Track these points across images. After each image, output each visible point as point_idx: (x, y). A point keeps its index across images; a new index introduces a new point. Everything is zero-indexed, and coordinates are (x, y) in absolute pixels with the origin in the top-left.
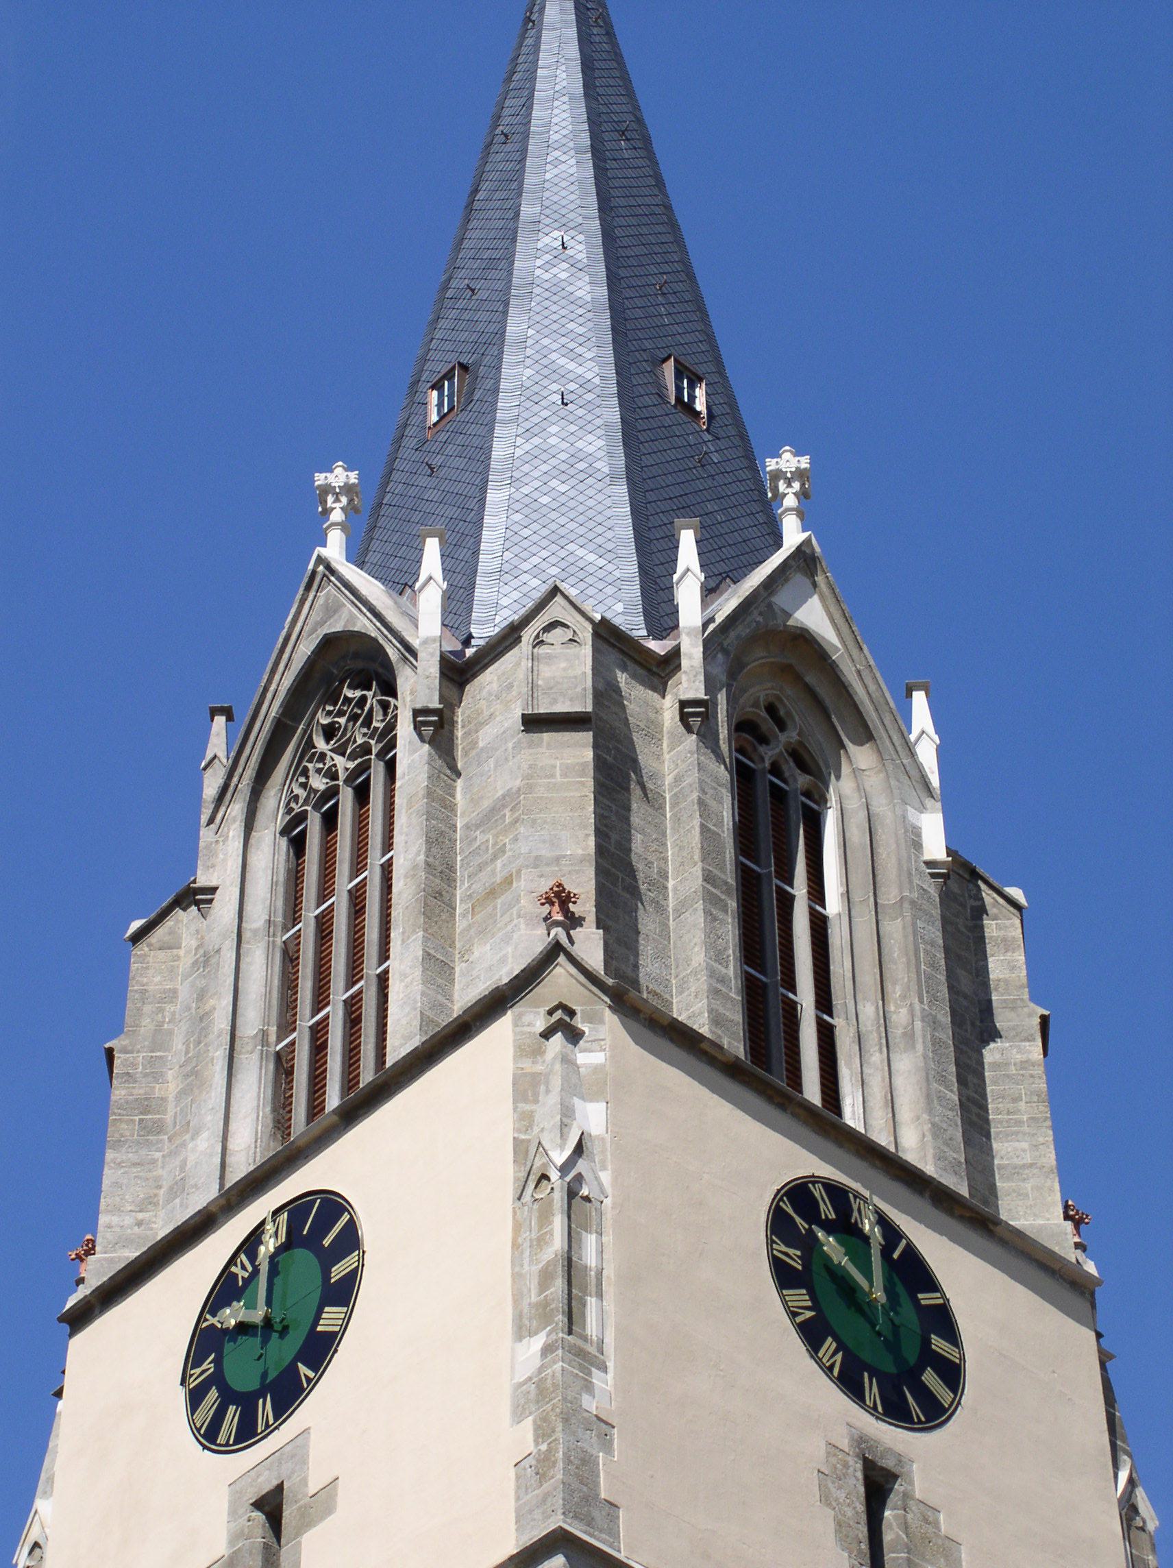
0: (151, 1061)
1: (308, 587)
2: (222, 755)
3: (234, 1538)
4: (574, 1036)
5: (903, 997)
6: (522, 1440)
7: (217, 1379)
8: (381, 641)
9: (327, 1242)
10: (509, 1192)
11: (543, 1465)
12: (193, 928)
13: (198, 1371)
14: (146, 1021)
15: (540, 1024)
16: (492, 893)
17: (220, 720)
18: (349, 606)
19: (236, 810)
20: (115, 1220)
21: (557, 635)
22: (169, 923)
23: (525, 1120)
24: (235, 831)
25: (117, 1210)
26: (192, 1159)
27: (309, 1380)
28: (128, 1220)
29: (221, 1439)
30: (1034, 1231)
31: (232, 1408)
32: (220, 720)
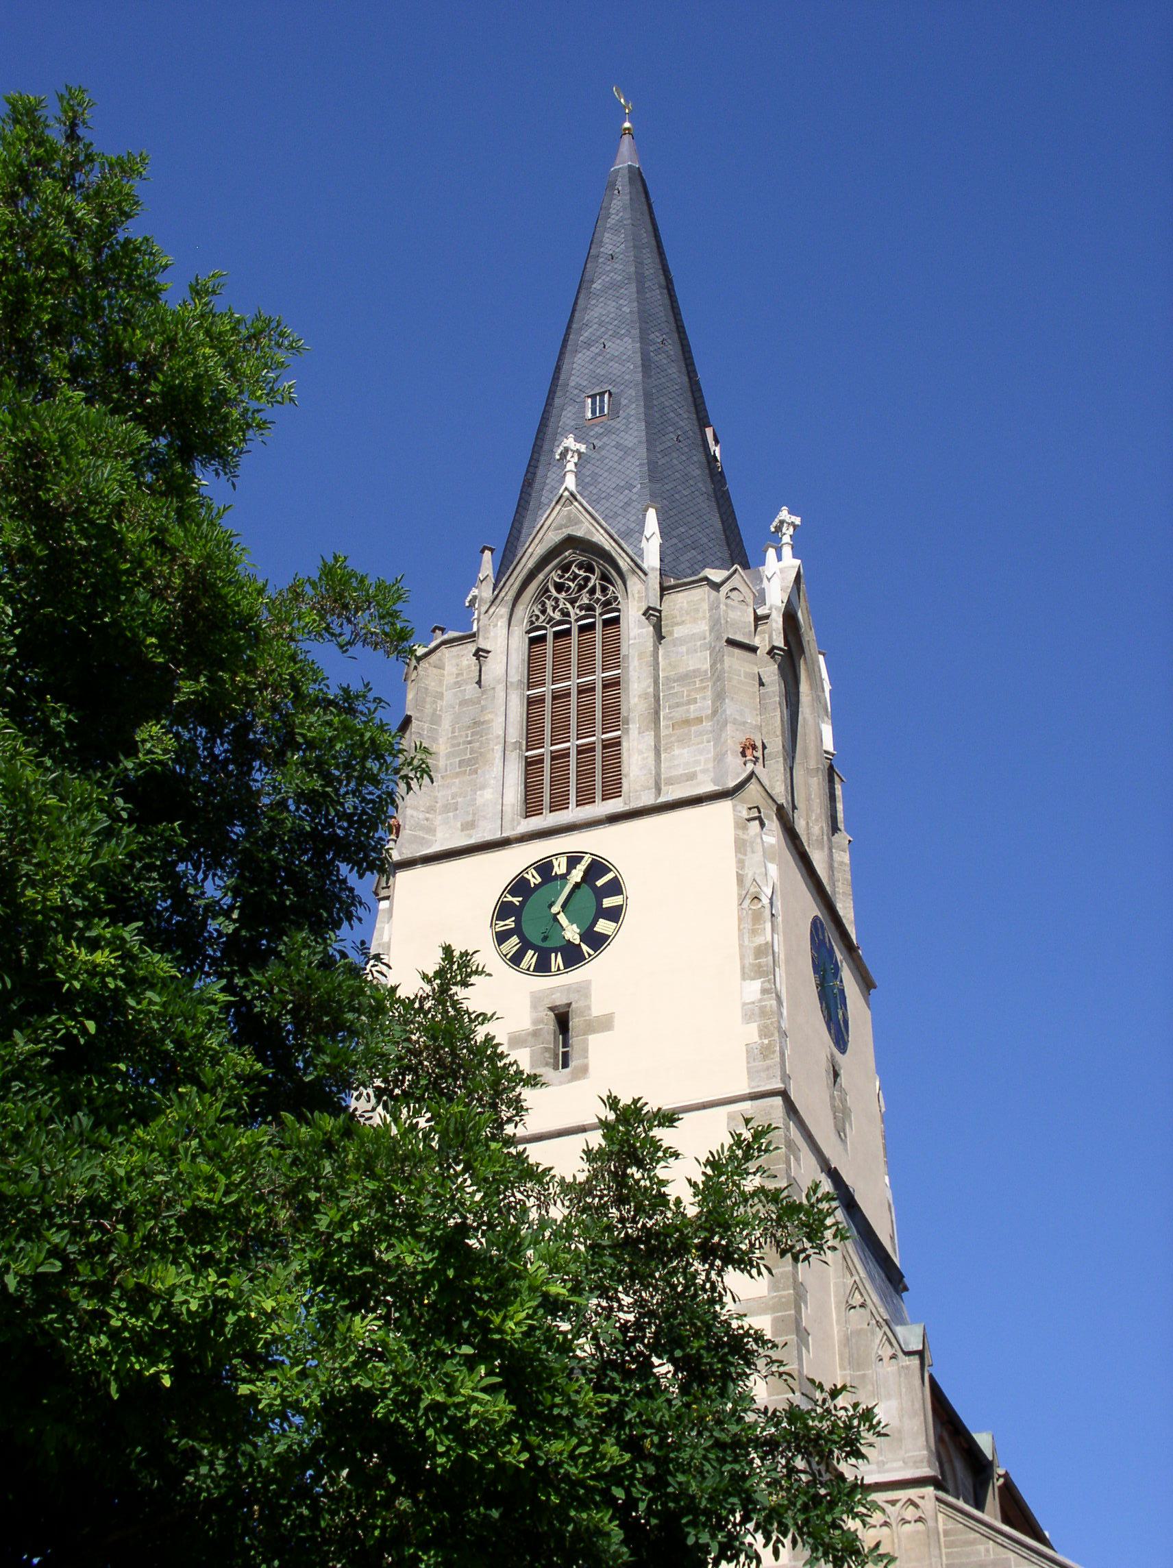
0: (431, 730)
1: (557, 502)
2: (491, 575)
3: (536, 1022)
4: (762, 825)
5: (817, 820)
6: (751, 1032)
7: (517, 931)
8: (614, 554)
9: (599, 883)
10: (735, 902)
11: (765, 1052)
12: (454, 662)
13: (502, 923)
14: (428, 706)
15: (745, 814)
16: (687, 722)
17: (487, 554)
18: (587, 524)
19: (503, 611)
20: (415, 813)
21: (734, 594)
22: (438, 653)
23: (741, 864)
24: (502, 623)
25: (415, 808)
26: (479, 801)
27: (590, 955)
28: (421, 816)
29: (524, 964)
30: (380, 833)
31: (530, 952)
32: (487, 554)
